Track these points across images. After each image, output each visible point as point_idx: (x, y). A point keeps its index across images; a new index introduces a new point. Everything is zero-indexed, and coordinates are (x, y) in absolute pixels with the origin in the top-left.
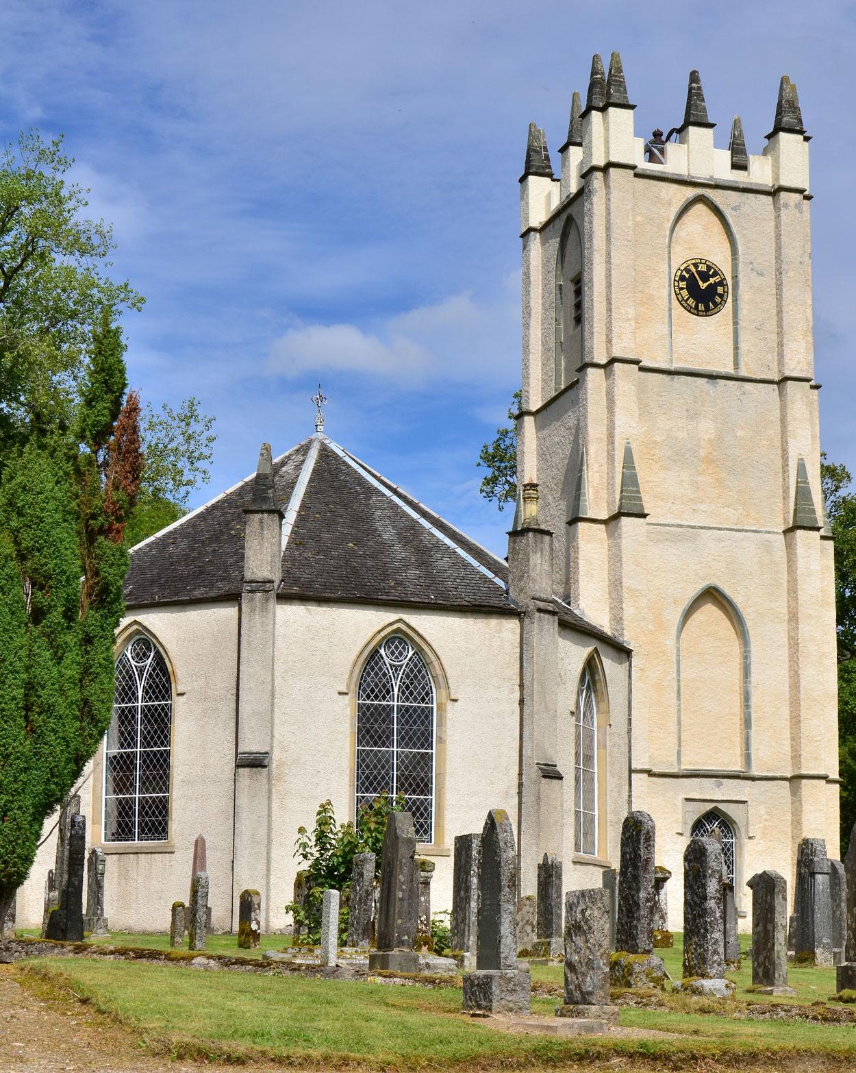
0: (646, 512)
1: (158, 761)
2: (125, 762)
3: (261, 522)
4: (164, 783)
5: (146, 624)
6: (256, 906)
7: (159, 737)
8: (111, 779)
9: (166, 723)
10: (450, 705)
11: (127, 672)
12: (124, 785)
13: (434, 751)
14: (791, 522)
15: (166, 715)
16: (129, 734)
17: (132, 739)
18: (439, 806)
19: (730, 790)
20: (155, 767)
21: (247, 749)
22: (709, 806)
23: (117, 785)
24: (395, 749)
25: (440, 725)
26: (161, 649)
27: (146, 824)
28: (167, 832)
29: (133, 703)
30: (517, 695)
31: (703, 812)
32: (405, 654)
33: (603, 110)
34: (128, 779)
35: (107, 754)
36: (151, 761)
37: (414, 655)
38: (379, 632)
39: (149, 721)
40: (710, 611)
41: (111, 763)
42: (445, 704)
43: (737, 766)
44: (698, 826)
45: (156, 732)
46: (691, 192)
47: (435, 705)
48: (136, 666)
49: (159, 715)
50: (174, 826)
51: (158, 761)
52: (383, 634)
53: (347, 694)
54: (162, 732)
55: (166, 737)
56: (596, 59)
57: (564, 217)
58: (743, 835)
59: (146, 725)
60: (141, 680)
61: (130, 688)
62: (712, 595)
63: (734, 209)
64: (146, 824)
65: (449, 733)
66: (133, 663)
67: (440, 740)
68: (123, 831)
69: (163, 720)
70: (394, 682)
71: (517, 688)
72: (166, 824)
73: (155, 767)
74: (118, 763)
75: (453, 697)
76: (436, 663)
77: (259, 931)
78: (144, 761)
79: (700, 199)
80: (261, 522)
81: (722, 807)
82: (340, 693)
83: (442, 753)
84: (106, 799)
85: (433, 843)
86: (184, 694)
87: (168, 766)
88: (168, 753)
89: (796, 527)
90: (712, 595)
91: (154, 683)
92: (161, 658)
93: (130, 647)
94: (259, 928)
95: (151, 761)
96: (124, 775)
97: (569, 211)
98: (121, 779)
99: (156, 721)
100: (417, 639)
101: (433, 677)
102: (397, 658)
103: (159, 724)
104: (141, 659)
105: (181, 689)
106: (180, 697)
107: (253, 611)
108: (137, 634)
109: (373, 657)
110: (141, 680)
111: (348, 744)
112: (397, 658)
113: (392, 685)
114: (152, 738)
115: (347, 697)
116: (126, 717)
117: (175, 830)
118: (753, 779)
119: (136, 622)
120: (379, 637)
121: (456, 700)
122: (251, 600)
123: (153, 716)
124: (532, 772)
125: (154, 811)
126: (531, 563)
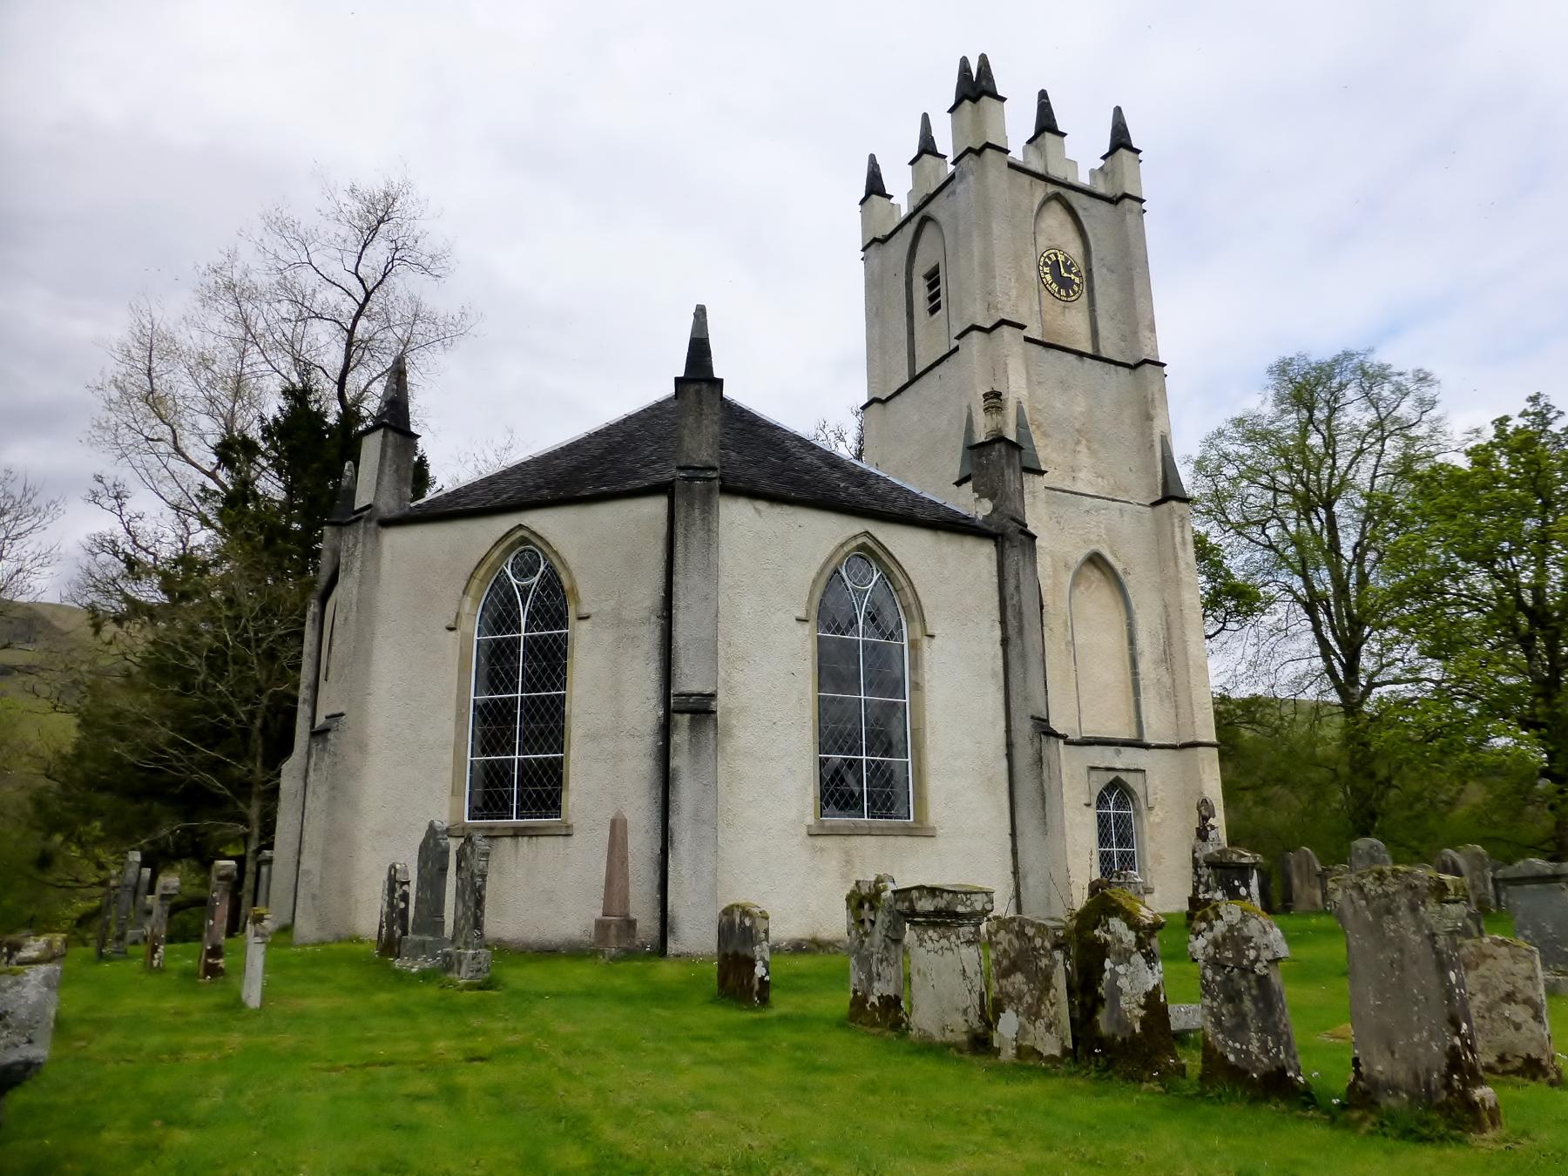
0: (1043, 468)
1: (548, 709)
2: (500, 712)
3: (698, 392)
4: (556, 740)
5: (535, 528)
6: (763, 935)
7: (549, 678)
8: (478, 733)
9: (559, 659)
10: (925, 640)
11: (506, 594)
12: (498, 742)
13: (907, 700)
14: (1160, 493)
15: (560, 647)
16: (507, 674)
17: (511, 680)
18: (919, 771)
19: (1129, 758)
20: (542, 717)
21: (685, 689)
22: (1111, 776)
23: (488, 742)
24: (862, 696)
25: (915, 665)
26: (556, 562)
27: (529, 796)
28: (560, 808)
29: (514, 633)
30: (998, 634)
31: (1107, 782)
32: (869, 577)
33: (975, 100)
34: (503, 734)
35: (475, 700)
36: (538, 710)
37: (879, 579)
38: (842, 546)
39: (535, 657)
40: (1094, 575)
41: (481, 713)
42: (920, 641)
43: (1128, 734)
44: (1102, 801)
45: (544, 671)
46: (1051, 189)
47: (906, 643)
48: (517, 585)
49: (550, 648)
50: (573, 798)
51: (548, 709)
52: (846, 549)
53: (807, 621)
54: (554, 671)
55: (559, 677)
56: (964, 61)
57: (916, 219)
58: (1143, 807)
59: (530, 662)
60: (524, 603)
61: (509, 614)
62: (1096, 560)
63: (1085, 209)
64: (529, 796)
65: (927, 677)
66: (514, 581)
67: (916, 686)
68: (496, 805)
69: (555, 655)
70: (857, 612)
71: (998, 625)
72: (559, 796)
73: (542, 717)
74: (490, 712)
75: (929, 632)
76: (907, 590)
77: (767, 978)
78: (528, 711)
79: (1057, 197)
80: (698, 392)
81: (1123, 776)
82: (798, 620)
83: (918, 706)
84: (472, 762)
85: (912, 820)
86: (588, 617)
87: (563, 716)
88: (562, 699)
89: (1164, 500)
90: (1096, 560)
91: (543, 606)
92: (555, 574)
93: (511, 561)
94: (768, 973)
95: (538, 710)
96: (499, 729)
97: (924, 211)
98: (494, 735)
99: (545, 657)
100: (885, 558)
101: (903, 607)
102: (860, 581)
103: (549, 661)
104: (525, 576)
105: (584, 611)
106: (582, 622)
107: (691, 505)
108: (521, 544)
109: (834, 578)
110: (524, 603)
111: (811, 689)
112: (860, 581)
113: (856, 614)
114: (539, 679)
115: (807, 626)
116: (503, 652)
117: (573, 805)
118: (1147, 747)
119: (520, 527)
120: (842, 553)
121: (932, 636)
122: (689, 489)
123: (540, 649)
124: (1024, 728)
125: (530, 778)
126: (1006, 477)
